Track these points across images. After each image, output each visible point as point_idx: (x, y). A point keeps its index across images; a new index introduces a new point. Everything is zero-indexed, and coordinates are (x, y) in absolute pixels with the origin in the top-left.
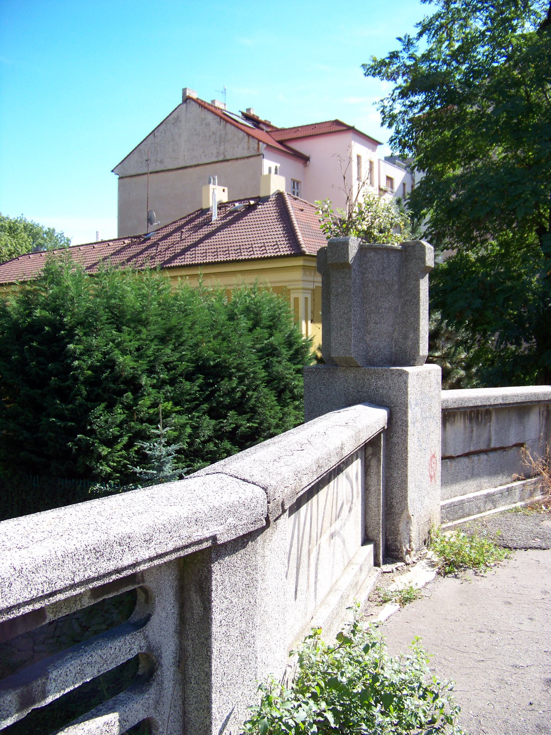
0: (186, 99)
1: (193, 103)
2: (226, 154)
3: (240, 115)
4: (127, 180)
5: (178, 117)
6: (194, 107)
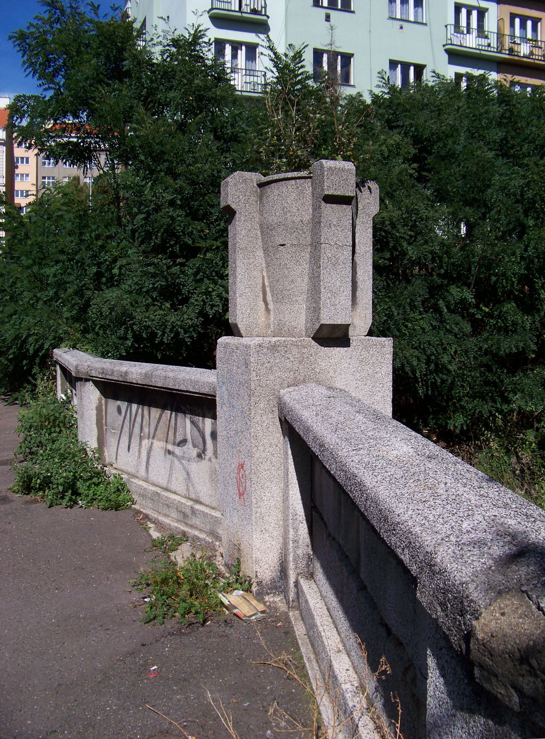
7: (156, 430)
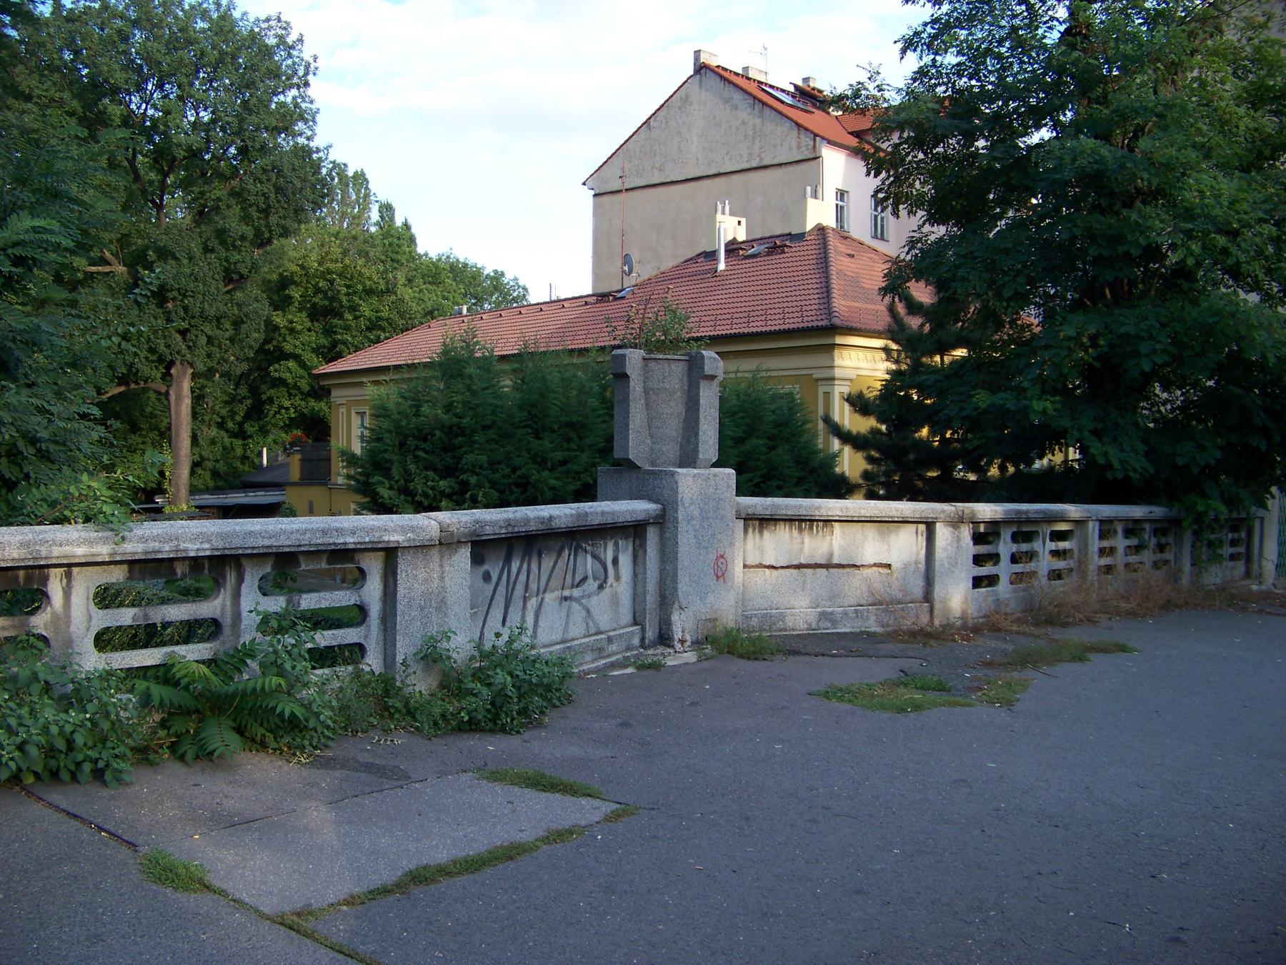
0: (701, 68)
1: (710, 74)
2: (763, 155)
3: (792, 89)
4: (606, 199)
5: (687, 97)
6: (712, 80)
7: (549, 580)
